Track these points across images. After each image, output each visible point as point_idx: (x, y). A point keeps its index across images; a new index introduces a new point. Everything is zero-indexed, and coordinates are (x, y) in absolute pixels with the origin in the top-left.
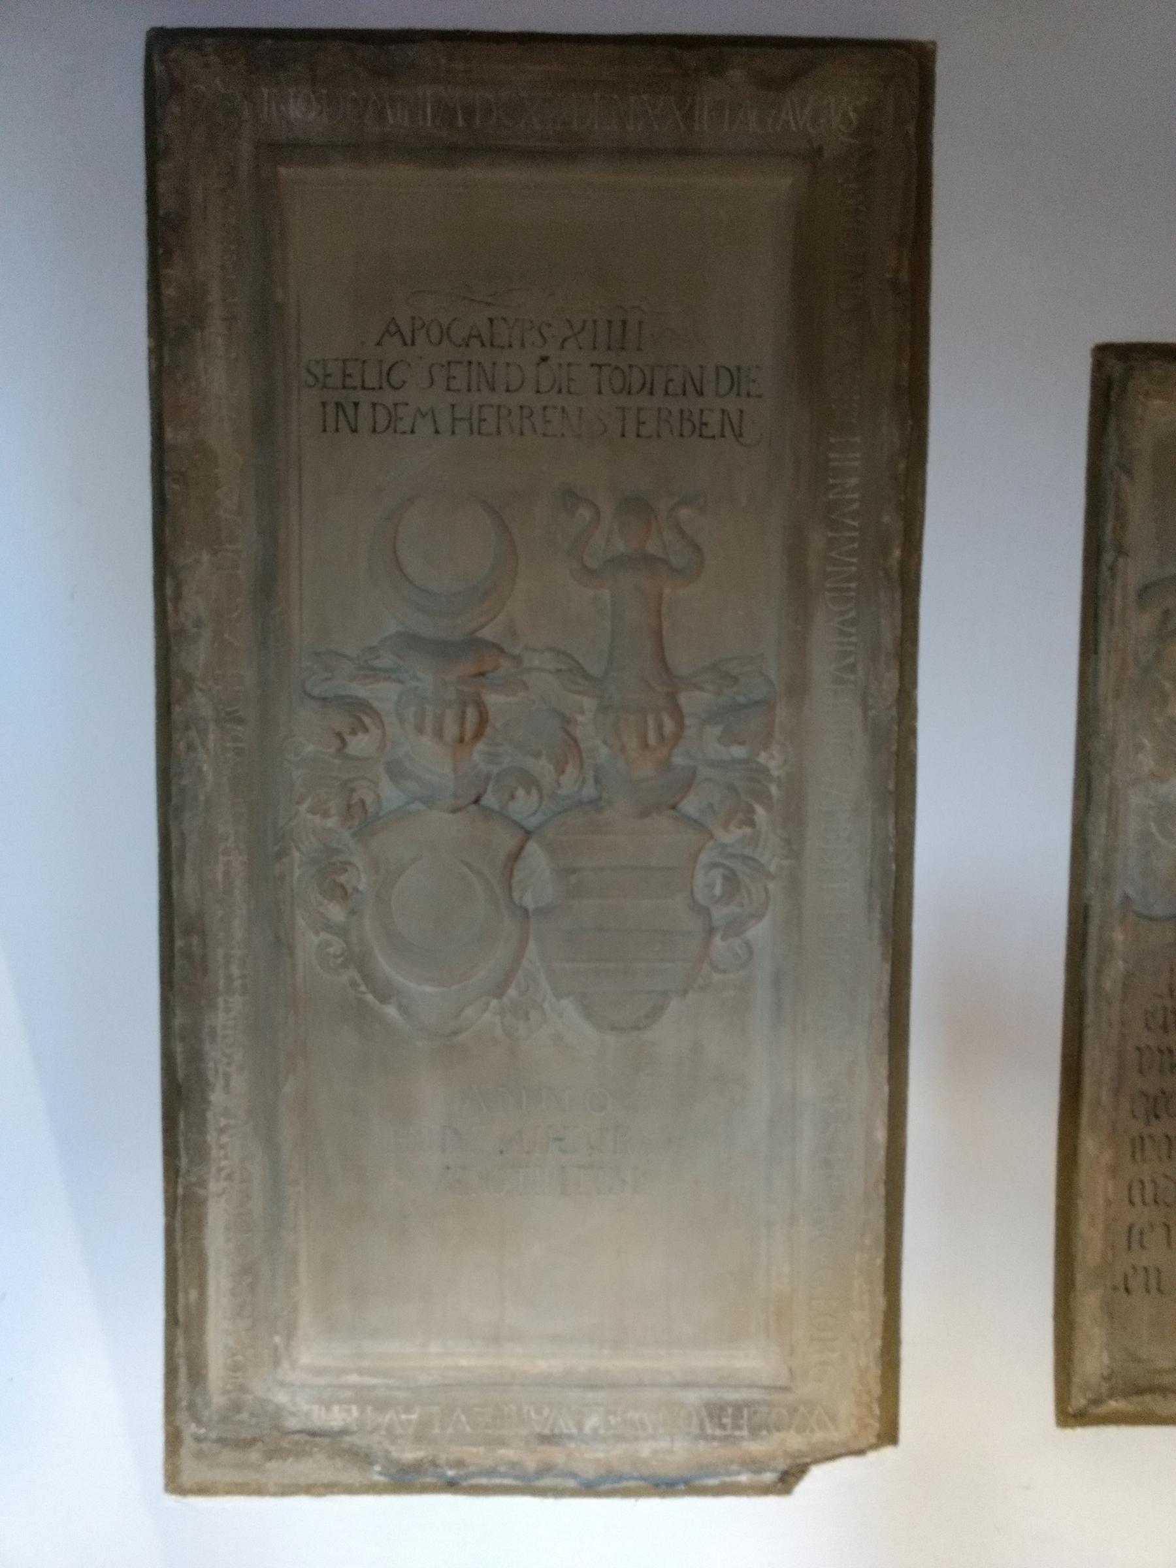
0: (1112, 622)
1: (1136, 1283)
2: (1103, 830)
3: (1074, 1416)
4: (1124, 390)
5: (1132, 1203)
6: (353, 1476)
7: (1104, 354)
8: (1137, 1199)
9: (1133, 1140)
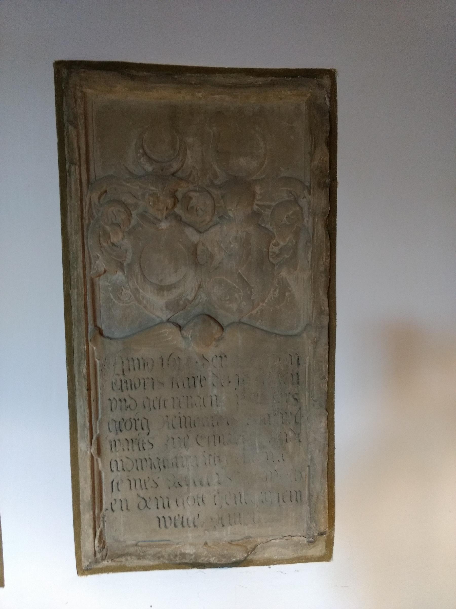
0: (71, 197)
1: (116, 507)
2: (76, 297)
3: (87, 570)
4: (67, 83)
5: (112, 471)
6: (136, 562)
7: (60, 66)
8: (114, 469)
9: (110, 442)
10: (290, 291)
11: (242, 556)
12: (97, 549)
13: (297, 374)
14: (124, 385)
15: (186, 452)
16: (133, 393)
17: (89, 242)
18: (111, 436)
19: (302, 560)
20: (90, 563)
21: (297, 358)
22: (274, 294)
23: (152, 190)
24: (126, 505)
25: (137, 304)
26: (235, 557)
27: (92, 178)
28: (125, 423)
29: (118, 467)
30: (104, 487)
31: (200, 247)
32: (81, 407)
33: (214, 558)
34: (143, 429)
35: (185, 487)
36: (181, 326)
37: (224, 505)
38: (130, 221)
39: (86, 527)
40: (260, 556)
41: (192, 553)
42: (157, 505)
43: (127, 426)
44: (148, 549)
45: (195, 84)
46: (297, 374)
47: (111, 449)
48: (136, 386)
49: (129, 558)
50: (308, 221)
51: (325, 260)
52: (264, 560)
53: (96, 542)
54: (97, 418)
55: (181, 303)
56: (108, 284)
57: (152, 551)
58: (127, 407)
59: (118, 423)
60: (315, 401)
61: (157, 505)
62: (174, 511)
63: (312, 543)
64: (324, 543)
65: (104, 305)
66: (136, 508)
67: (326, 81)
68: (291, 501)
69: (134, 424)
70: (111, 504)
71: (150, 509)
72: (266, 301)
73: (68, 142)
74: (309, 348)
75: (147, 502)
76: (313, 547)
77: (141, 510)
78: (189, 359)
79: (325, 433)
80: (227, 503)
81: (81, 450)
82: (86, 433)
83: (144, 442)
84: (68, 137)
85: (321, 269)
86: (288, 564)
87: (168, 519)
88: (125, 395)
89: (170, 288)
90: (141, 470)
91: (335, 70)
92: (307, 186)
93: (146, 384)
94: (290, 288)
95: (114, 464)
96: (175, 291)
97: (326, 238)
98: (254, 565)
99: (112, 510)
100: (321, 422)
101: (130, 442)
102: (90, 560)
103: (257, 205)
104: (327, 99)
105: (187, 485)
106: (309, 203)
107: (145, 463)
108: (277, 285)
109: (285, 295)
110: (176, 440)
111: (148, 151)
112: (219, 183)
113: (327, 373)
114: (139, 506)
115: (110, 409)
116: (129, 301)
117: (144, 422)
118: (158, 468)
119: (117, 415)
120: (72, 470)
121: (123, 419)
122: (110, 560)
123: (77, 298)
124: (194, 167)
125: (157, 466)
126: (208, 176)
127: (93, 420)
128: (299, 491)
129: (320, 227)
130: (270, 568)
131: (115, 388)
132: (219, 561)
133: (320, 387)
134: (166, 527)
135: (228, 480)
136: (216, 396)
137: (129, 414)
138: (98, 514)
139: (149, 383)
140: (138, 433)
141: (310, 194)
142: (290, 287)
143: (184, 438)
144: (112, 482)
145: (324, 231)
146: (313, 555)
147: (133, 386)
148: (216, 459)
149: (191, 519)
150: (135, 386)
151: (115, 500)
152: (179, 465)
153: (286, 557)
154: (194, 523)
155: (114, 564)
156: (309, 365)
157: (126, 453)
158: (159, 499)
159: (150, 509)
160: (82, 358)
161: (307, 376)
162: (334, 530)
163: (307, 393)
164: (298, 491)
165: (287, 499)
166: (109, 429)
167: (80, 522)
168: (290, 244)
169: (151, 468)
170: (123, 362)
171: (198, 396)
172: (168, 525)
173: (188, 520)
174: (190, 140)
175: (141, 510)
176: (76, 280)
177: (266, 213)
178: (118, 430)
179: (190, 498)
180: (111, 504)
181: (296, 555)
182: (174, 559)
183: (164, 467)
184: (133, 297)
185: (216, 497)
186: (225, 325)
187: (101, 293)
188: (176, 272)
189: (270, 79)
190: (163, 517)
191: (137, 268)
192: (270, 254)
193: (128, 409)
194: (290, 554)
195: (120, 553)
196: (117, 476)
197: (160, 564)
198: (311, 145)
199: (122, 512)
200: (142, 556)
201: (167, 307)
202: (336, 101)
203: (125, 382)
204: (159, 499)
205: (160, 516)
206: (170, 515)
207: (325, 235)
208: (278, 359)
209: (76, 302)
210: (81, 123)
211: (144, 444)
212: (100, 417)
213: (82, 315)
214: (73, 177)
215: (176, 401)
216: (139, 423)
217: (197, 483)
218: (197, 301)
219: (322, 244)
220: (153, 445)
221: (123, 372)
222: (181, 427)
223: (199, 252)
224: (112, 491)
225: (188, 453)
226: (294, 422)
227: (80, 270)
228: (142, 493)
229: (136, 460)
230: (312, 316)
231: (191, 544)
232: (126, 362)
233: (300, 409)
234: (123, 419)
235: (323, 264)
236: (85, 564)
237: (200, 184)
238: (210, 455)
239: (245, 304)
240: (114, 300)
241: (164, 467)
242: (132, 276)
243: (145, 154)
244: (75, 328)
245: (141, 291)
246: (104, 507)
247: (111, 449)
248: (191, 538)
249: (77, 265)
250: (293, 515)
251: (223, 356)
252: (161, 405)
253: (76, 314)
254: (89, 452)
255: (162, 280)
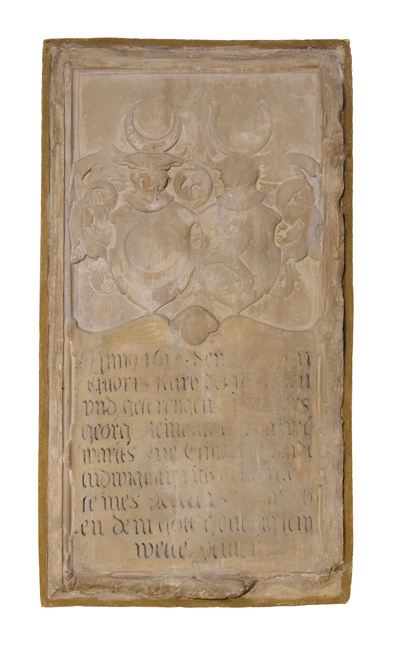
0: (54, 178)
2: (54, 285)
5: (84, 486)
6: (109, 596)
8: (87, 484)
10: (299, 280)
11: (238, 590)
12: (65, 575)
13: (308, 376)
14: (102, 386)
15: (171, 466)
16: (112, 395)
17: (70, 226)
18: (85, 444)
19: (312, 601)
20: (57, 590)
21: (307, 358)
22: (280, 284)
23: (142, 170)
24: (99, 527)
25: (119, 294)
26: (229, 591)
27: (76, 157)
28: (102, 430)
29: (92, 482)
30: (73, 505)
31: (195, 231)
32: (54, 407)
33: (204, 591)
34: (122, 437)
35: (170, 509)
36: (170, 319)
37: (218, 532)
38: (115, 202)
39: (54, 547)
40: (260, 595)
41: (177, 585)
42: (137, 529)
43: (103, 434)
44: (124, 580)
45: (193, 58)
46: (308, 376)
47: (85, 460)
48: (116, 387)
49: (101, 591)
50: (319, 202)
51: (339, 245)
52: (264, 600)
53: (65, 566)
54: (70, 423)
55: (171, 292)
56: (87, 271)
57: (128, 583)
58: (104, 411)
59: (93, 430)
60: (328, 407)
61: (137, 529)
62: (156, 538)
63: (325, 581)
64: (340, 580)
65: (82, 294)
66: (112, 533)
67: (340, 52)
68: (300, 530)
69: (112, 431)
70: (82, 525)
71: (127, 533)
72: (271, 292)
73: (54, 121)
74: (322, 345)
75: (125, 525)
76: (326, 585)
77: (117, 534)
78: (178, 356)
79: (340, 444)
80: (220, 530)
81: (52, 457)
82: (58, 437)
83: (123, 453)
84: (54, 115)
85: (334, 255)
86: (295, 605)
87: (148, 547)
88: (103, 397)
89: (158, 276)
90: (119, 486)
91: (349, 40)
92: (318, 163)
93: (127, 386)
94: (300, 277)
95: (87, 477)
96: (164, 279)
97: (340, 220)
98: (253, 606)
99: (83, 533)
100: (334, 432)
101: (107, 452)
102: (57, 588)
103: (261, 183)
104: (340, 71)
105: (173, 506)
106: (320, 182)
107: (124, 477)
108: (283, 273)
109: (294, 285)
110: (162, 451)
111: (138, 127)
112: (218, 160)
113: (342, 374)
114: (115, 530)
115: (85, 413)
116: (110, 291)
117: (124, 428)
118: (138, 485)
119: (93, 420)
120: (39, 481)
121: (99, 425)
122: (79, 591)
123: (56, 286)
124: (189, 144)
125: (137, 482)
126: (205, 152)
127: (65, 424)
128: (310, 517)
129: (333, 209)
130: (272, 609)
131: (92, 389)
132: (210, 595)
133: (334, 390)
134: (146, 556)
135: (222, 501)
136: (209, 400)
137: (106, 420)
138: (67, 535)
139: (131, 383)
140: (116, 441)
141: (321, 173)
142: (299, 275)
143: (171, 450)
144: (84, 500)
145: (337, 213)
146: (326, 596)
147: (112, 387)
148: (209, 474)
149: (176, 548)
150: (115, 387)
151: (86, 521)
152: (164, 481)
153: (293, 597)
154: (180, 553)
155: (84, 596)
156: (322, 365)
157: (102, 465)
158: (139, 522)
159: (127, 533)
160: (57, 353)
161: (319, 378)
162: (351, 565)
163: (319, 398)
164: (307, 517)
165: (294, 526)
166: (83, 436)
167: (47, 542)
168: (299, 227)
169: (131, 484)
170: (102, 360)
171: (189, 400)
172: (148, 554)
173: (172, 548)
174: (185, 115)
175: (117, 534)
176: (55, 266)
177: (272, 193)
178: (93, 437)
179: (175, 522)
180: (82, 525)
181: (304, 596)
182: (155, 593)
183: (146, 483)
184: (115, 286)
185: (208, 521)
186: (221, 319)
187: (79, 281)
188: (166, 258)
189: (276, 50)
190: (143, 544)
191: (121, 253)
192: (276, 238)
193: (106, 413)
194: (297, 593)
195: (90, 583)
196: (90, 492)
197: (138, 600)
198: (323, 119)
199: (94, 536)
200: (117, 588)
201: (154, 297)
202: (351, 72)
203: (103, 382)
204: (139, 522)
205: (140, 543)
206: (151, 541)
207: (338, 217)
208: (285, 359)
209: (54, 290)
210: (67, 100)
211: (123, 455)
212: (73, 422)
213: (60, 304)
214: (57, 157)
215: (163, 406)
216: (117, 430)
217: (186, 504)
218: (189, 291)
219: (334, 227)
220: (133, 457)
221: (102, 371)
222: (167, 436)
223: (192, 237)
224: (84, 511)
225: (174, 468)
226: (303, 432)
227: (60, 255)
228: (119, 514)
229: (113, 474)
230: (325, 309)
231: (176, 577)
232: (105, 359)
233: (310, 417)
234: (99, 425)
235: (337, 249)
236: (51, 591)
237: (195, 162)
238: (201, 470)
239: (246, 295)
240: (94, 289)
241: (146, 483)
242: (115, 262)
243: (135, 130)
244: (51, 319)
245: (125, 279)
246: (73, 530)
247: (85, 460)
248: (176, 570)
249: (57, 249)
250: (302, 546)
251: (219, 354)
252: (144, 409)
253: (54, 303)
254: (60, 460)
255: (149, 267)
